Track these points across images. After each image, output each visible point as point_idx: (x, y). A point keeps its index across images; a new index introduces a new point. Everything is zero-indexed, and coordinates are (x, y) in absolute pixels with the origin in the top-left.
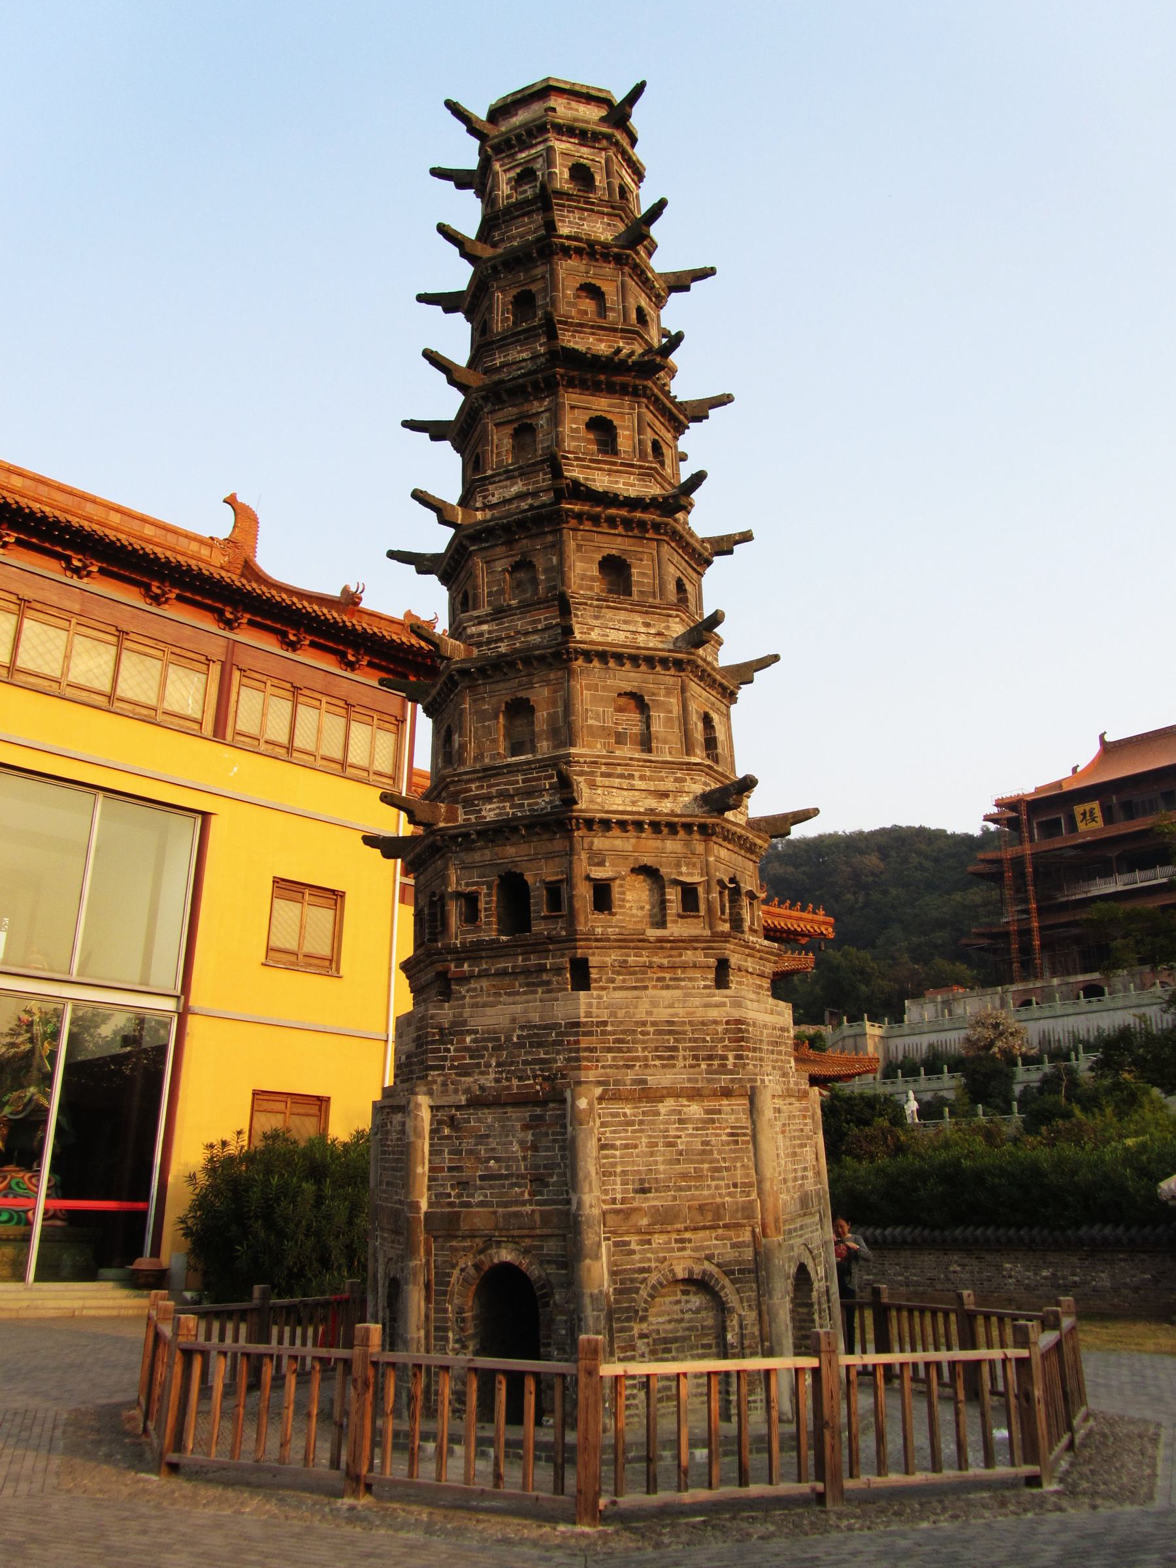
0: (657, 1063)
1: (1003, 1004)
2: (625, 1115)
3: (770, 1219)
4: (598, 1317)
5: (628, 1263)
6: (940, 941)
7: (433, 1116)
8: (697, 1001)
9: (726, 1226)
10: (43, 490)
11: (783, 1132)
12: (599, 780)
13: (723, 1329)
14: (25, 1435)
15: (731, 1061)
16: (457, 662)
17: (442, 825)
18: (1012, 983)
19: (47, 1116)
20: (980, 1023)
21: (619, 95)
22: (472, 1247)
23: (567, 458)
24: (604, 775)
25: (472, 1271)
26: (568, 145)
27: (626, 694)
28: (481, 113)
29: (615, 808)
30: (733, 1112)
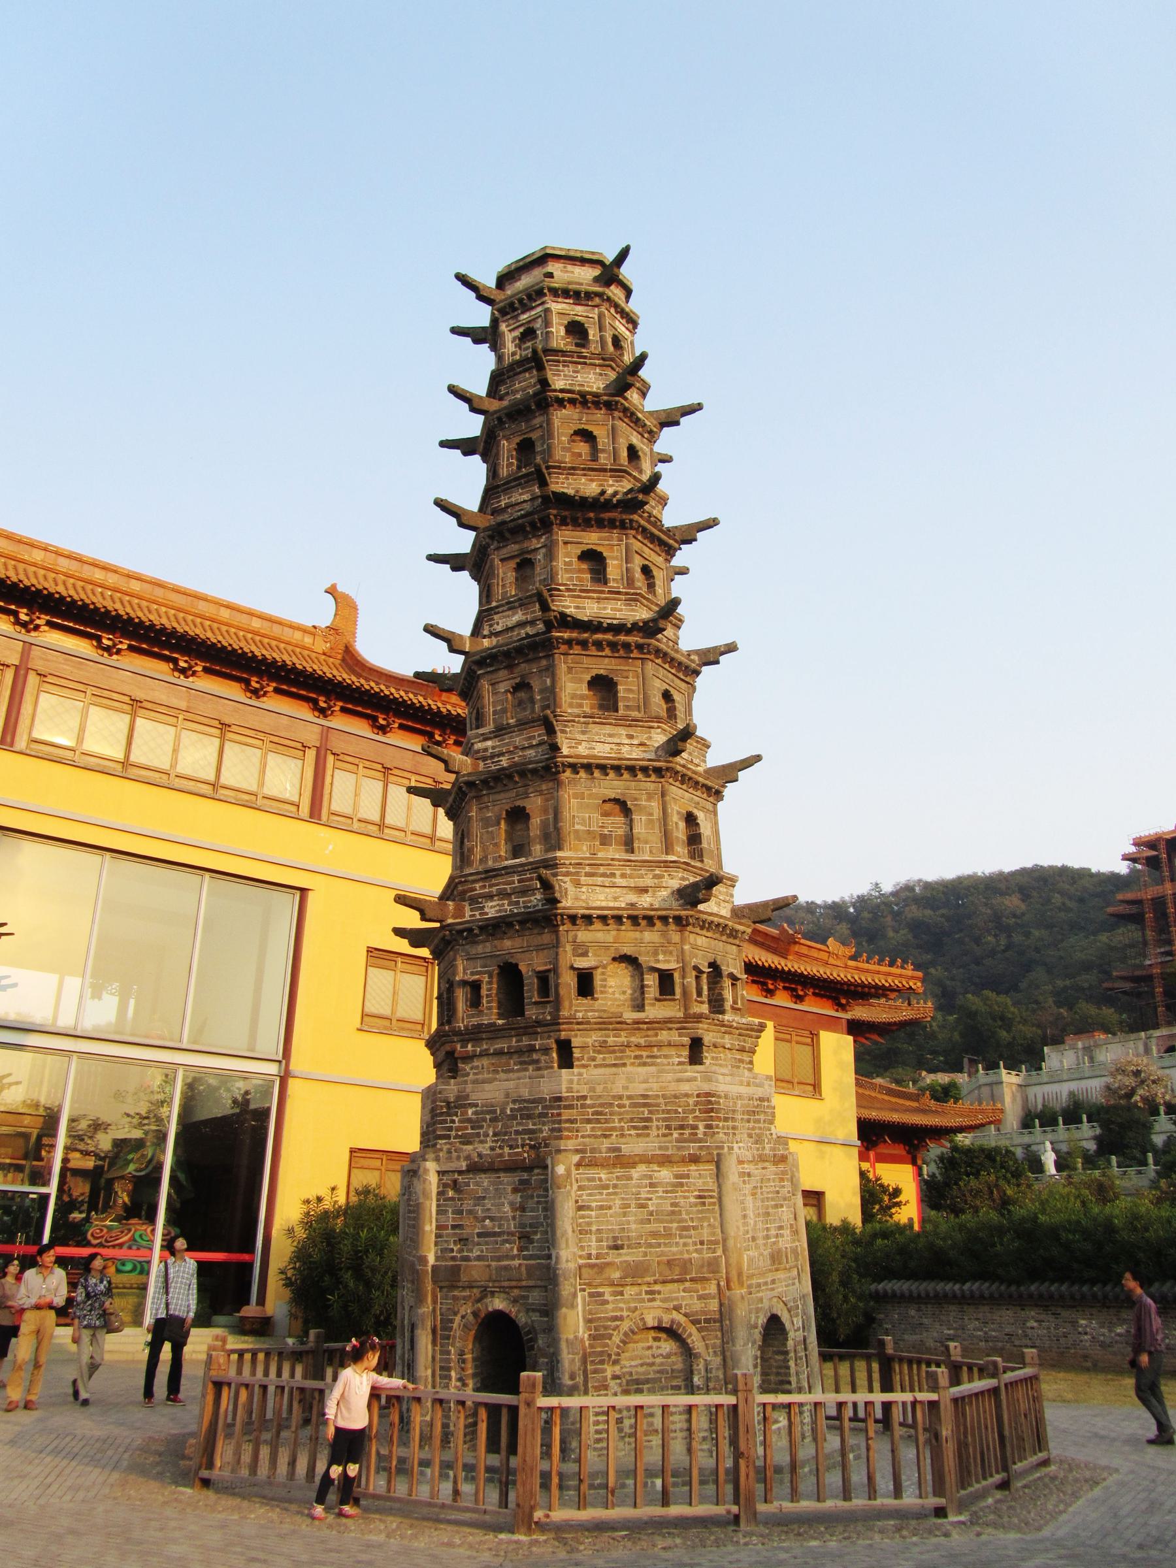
0: (633, 1132)
1: (1147, 1051)
2: (600, 1179)
3: (734, 1274)
4: (573, 1360)
5: (602, 1312)
6: (1086, 985)
7: (440, 1180)
8: (670, 1076)
9: (692, 1280)
10: (159, 592)
11: (754, 1194)
12: (583, 879)
13: (689, 1373)
14: (99, 1456)
15: (701, 1129)
16: (464, 775)
17: (450, 921)
18: (1156, 1026)
19: (161, 1173)
20: (1121, 1071)
21: (610, 256)
22: (470, 1296)
23: (559, 590)
24: (588, 875)
25: (471, 1318)
26: (564, 306)
27: (610, 800)
28: (488, 281)
29: (598, 904)
30: (701, 1177)
